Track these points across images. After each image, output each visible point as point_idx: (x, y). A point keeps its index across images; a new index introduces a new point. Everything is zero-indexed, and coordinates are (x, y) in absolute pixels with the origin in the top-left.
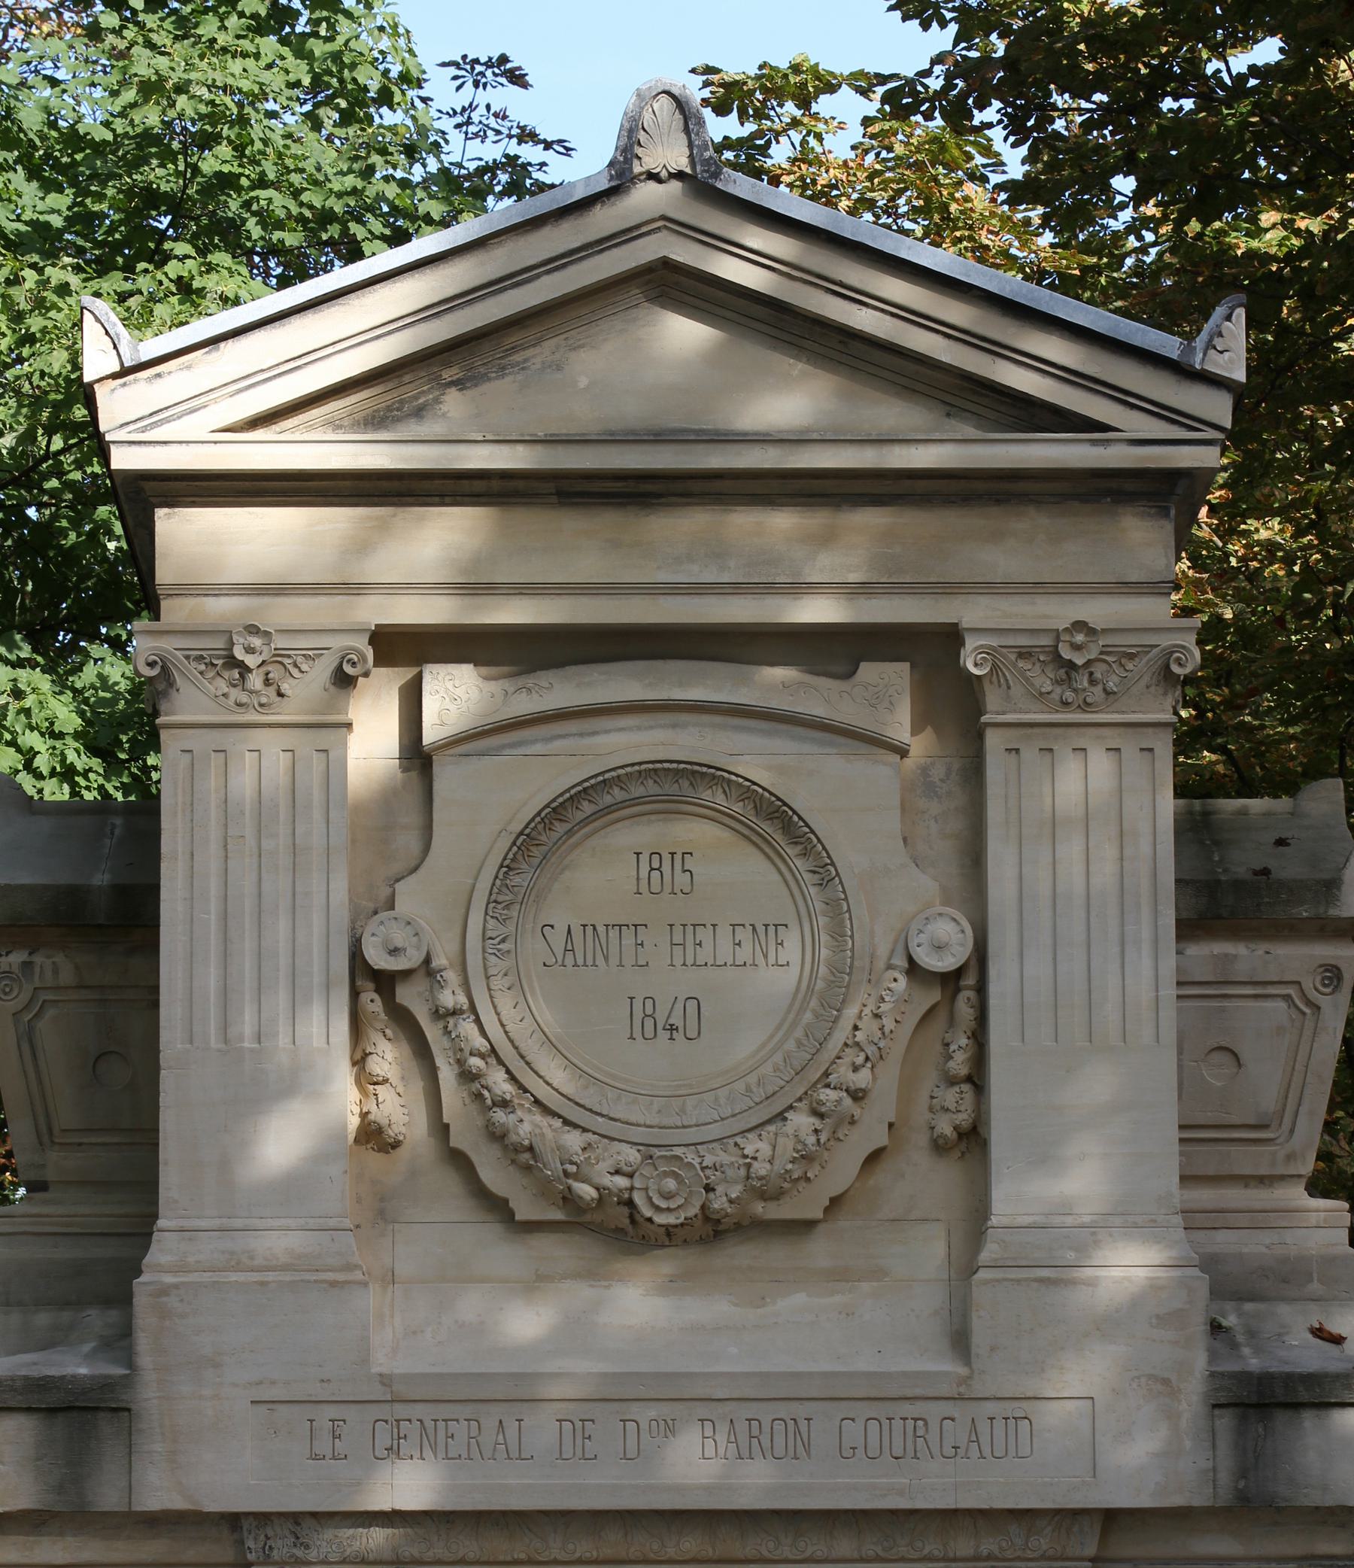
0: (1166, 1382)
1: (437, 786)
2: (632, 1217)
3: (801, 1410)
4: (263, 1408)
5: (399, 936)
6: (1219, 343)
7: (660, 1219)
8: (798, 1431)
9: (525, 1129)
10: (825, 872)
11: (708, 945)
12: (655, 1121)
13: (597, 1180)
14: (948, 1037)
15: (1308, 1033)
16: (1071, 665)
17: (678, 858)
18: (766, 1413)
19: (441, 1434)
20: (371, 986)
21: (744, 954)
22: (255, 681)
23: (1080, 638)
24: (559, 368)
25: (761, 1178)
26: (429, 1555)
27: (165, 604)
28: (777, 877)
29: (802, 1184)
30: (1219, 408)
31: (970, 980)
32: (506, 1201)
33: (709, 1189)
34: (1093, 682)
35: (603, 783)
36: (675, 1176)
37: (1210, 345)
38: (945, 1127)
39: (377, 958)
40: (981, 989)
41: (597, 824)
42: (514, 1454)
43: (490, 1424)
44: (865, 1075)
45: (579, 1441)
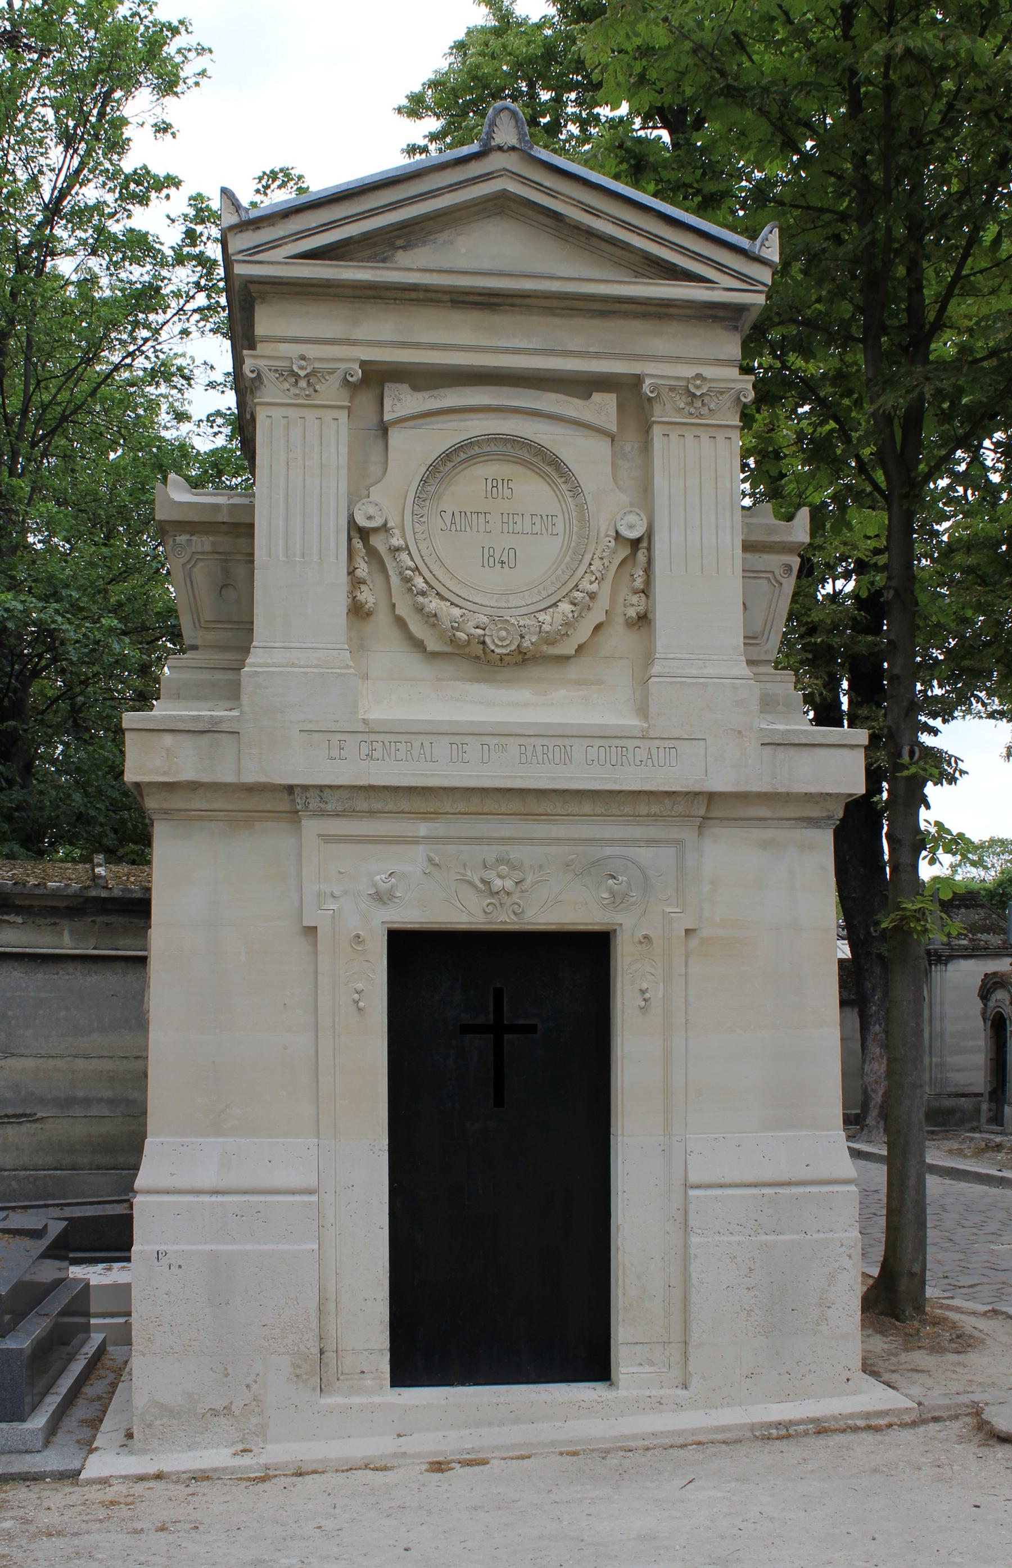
0: (740, 732)
1: (390, 442)
2: (484, 649)
3: (568, 742)
4: (305, 734)
5: (372, 511)
6: (767, 244)
7: (498, 651)
8: (566, 751)
9: (433, 605)
10: (576, 490)
11: (519, 523)
12: (495, 605)
13: (468, 631)
14: (633, 572)
15: (776, 595)
16: (694, 395)
17: (505, 482)
18: (550, 742)
19: (393, 748)
20: (358, 535)
21: (537, 529)
22: (303, 384)
23: (698, 382)
24: (452, 244)
25: (547, 632)
26: (386, 809)
27: (259, 346)
28: (552, 493)
29: (565, 638)
30: (765, 276)
31: (644, 544)
32: (422, 642)
33: (522, 637)
34: (703, 404)
35: (469, 444)
36: (506, 629)
37: (762, 245)
38: (632, 613)
39: (361, 521)
40: (649, 549)
41: (464, 466)
42: (428, 759)
43: (417, 744)
44: (595, 585)
45: (460, 754)
